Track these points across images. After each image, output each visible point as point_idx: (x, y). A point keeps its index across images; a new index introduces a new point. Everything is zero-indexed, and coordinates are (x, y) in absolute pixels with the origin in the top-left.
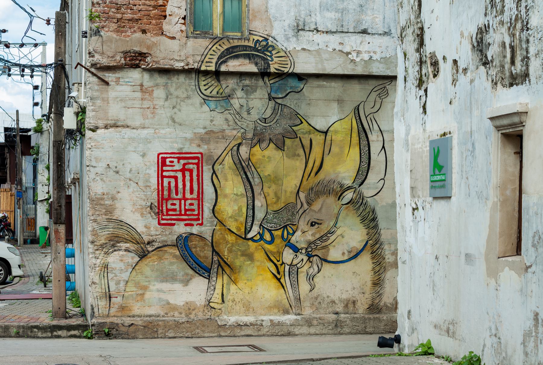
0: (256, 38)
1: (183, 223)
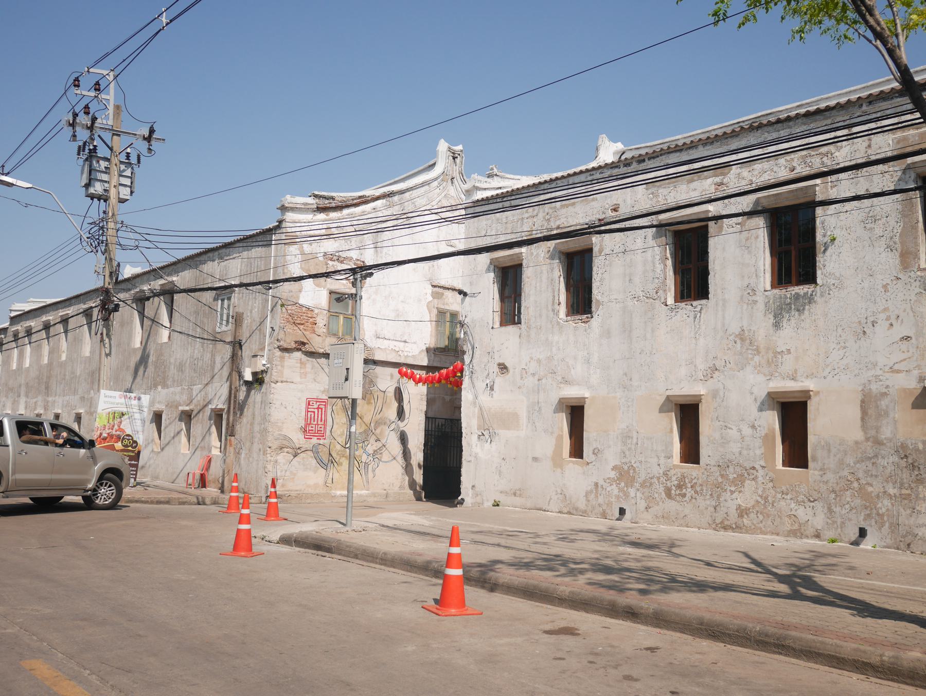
1: (316, 438)
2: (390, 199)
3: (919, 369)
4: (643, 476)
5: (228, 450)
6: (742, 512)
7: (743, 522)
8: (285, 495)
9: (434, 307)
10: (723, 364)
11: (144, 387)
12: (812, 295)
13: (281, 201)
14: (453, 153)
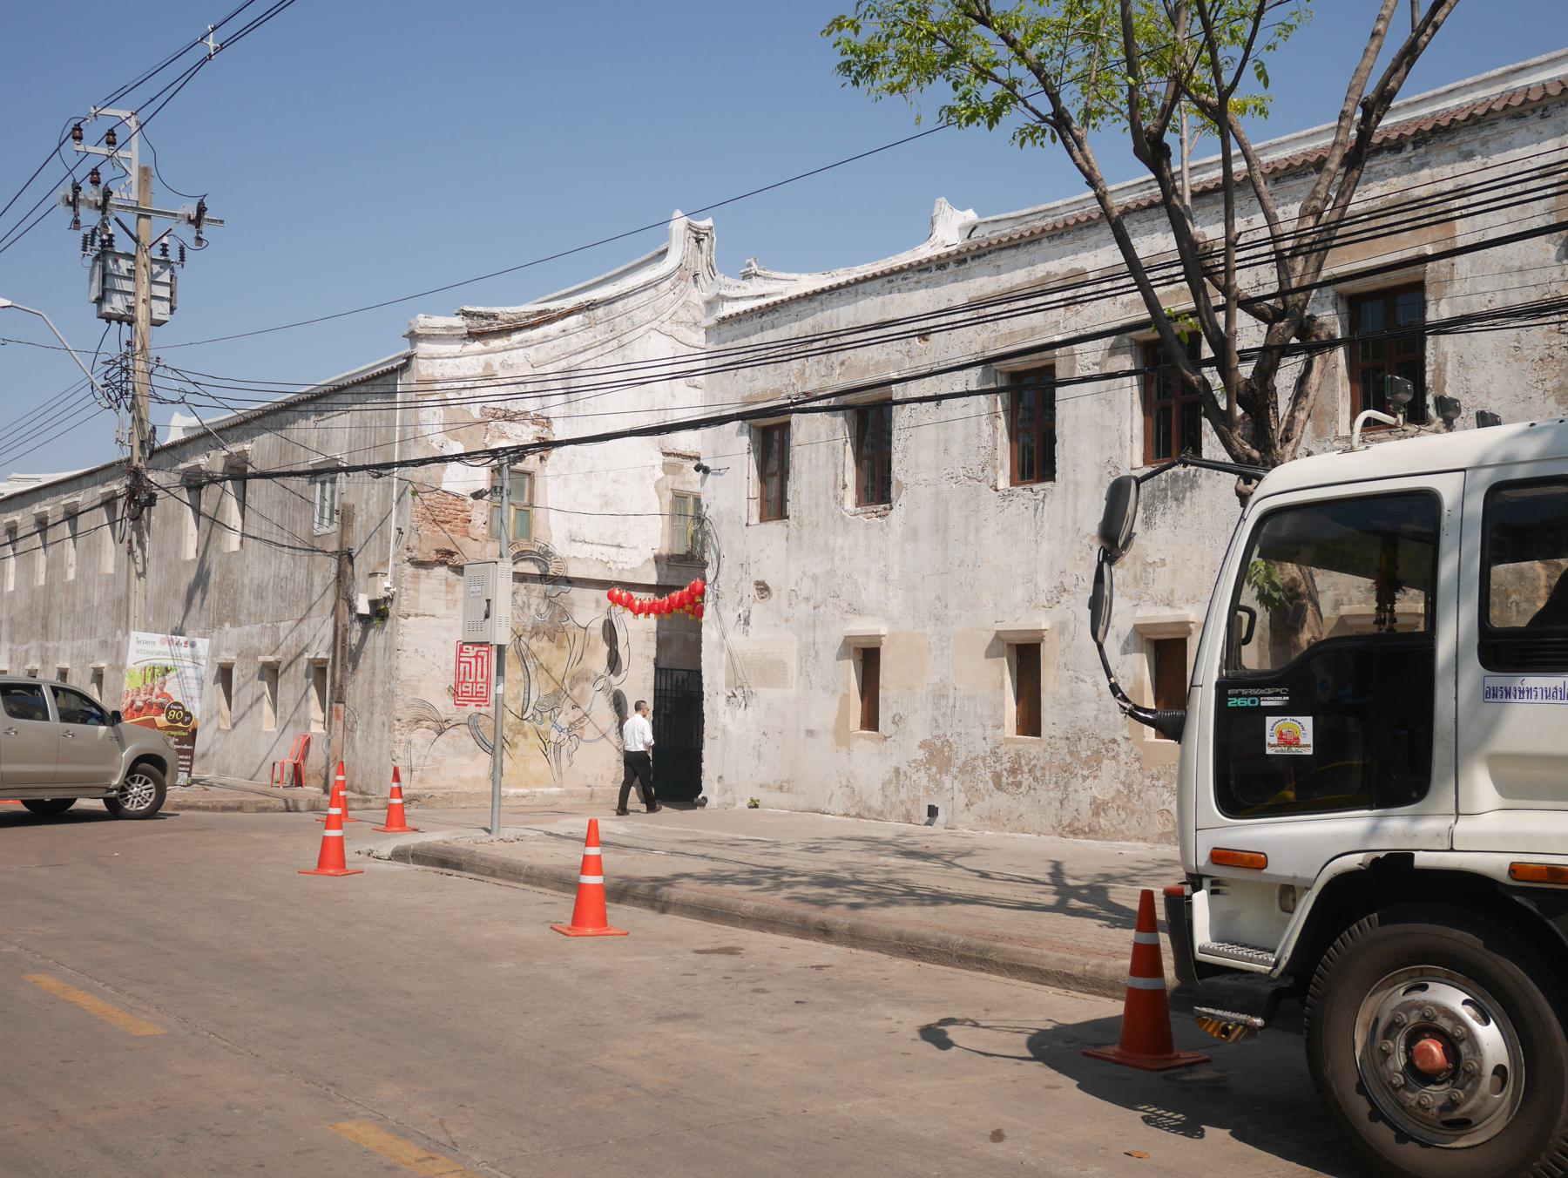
0: (540, 545)
1: (474, 704)
2: (591, 313)
3: (1335, 589)
4: (962, 756)
5: (333, 726)
6: (1098, 808)
7: (1099, 822)
8: (424, 796)
9: (667, 488)
10: (1075, 582)
11: (203, 624)
12: (1195, 476)
13: (410, 324)
14: (697, 233)
